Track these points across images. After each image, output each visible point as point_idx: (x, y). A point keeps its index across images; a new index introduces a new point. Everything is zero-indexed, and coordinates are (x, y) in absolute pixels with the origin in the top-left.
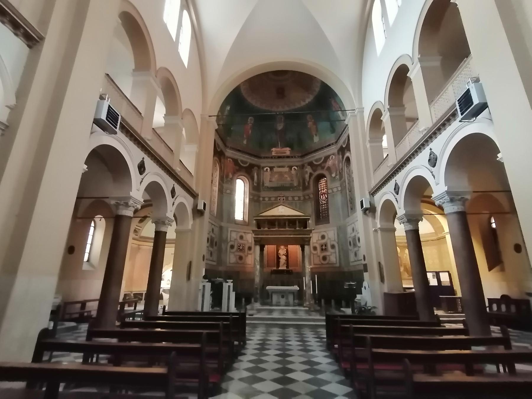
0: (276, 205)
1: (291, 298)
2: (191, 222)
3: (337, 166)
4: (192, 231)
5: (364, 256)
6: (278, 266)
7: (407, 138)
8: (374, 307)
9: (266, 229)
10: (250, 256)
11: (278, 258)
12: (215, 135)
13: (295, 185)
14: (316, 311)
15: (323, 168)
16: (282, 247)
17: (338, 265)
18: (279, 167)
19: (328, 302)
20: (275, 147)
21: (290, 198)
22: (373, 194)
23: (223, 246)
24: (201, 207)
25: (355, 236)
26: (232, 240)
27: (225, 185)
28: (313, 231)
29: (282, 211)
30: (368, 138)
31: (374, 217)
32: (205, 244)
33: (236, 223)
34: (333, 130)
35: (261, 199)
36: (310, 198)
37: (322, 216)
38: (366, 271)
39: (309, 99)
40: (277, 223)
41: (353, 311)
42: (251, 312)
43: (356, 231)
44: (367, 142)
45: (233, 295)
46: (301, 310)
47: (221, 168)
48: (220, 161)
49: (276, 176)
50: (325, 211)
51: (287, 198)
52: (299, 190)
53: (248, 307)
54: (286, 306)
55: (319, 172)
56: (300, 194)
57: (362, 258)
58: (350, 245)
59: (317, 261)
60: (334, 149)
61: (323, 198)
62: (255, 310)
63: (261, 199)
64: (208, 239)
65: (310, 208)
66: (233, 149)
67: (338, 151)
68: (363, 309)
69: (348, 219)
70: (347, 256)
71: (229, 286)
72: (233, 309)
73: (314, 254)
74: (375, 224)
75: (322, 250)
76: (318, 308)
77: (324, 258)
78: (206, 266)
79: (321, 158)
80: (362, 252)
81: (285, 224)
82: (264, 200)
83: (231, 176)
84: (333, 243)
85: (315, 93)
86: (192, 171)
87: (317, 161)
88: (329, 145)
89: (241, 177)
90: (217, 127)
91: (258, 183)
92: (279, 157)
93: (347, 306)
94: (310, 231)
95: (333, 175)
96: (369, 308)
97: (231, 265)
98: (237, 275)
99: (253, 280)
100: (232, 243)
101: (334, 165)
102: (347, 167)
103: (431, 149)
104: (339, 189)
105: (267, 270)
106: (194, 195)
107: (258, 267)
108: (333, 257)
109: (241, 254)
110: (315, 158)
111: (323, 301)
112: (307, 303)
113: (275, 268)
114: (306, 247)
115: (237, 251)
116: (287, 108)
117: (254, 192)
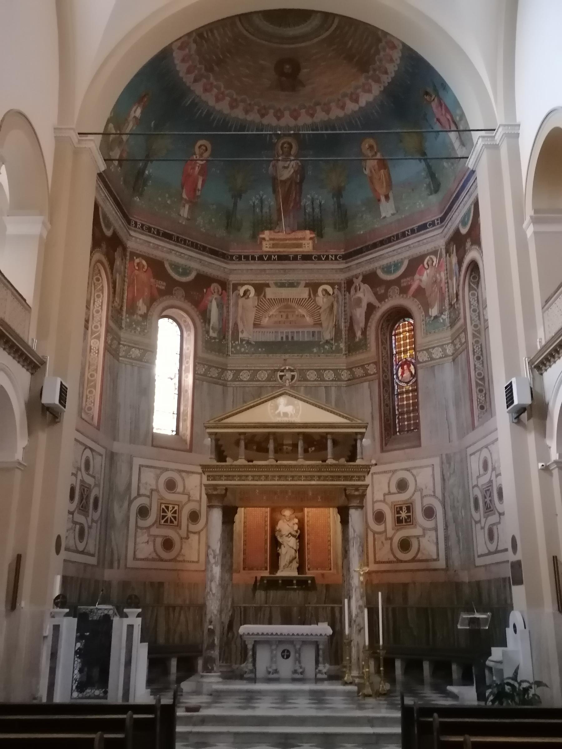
0: (270, 395)
1: (309, 655)
2: (22, 442)
4: (26, 468)
5: (514, 540)
6: (275, 566)
8: (539, 684)
9: (242, 461)
10: (194, 538)
11: (276, 544)
12: (98, 189)
13: (327, 336)
14: (378, 694)
15: (404, 291)
16: (287, 513)
17: (442, 564)
18: (282, 285)
19: (413, 667)
20: (271, 229)
21: (311, 375)
22: (540, 365)
23: (118, 515)
24: (51, 397)
25: (491, 481)
26: (142, 491)
27: (124, 335)
28: (373, 469)
29: (287, 410)
30: (529, 211)
31: (542, 431)
32: (63, 504)
33: (157, 442)
34: (435, 187)
36: (367, 375)
37: (398, 425)
38: (518, 581)
40: (271, 446)
41: (481, 696)
42: (194, 701)
43: (494, 469)
45: (141, 653)
46: (334, 693)
48: (112, 263)
49: (273, 311)
50: (408, 412)
51: (302, 372)
52: (339, 351)
53: (186, 686)
54: (294, 680)
55: (395, 300)
57: (509, 546)
59: (384, 554)
60: (436, 239)
61: (403, 375)
62: (205, 695)
63: (230, 375)
64: (72, 490)
65: (365, 406)
67: (448, 244)
68: (507, 688)
69: (472, 436)
70: (468, 542)
71: (130, 627)
72: (141, 694)
73: (374, 533)
74: (543, 452)
75: (399, 521)
76: (387, 687)
77: (405, 545)
78: (65, 568)
79: (402, 262)
80: (509, 527)
81: (295, 446)
82: (236, 378)
84: (428, 501)
85: (386, 79)
86: (27, 290)
87: (387, 269)
88: (423, 227)
90: (102, 167)
91: (223, 332)
92: (282, 258)
93: (466, 680)
94: (367, 469)
95: (434, 312)
96: (525, 685)
97: (139, 564)
98: (153, 595)
99: (201, 609)
102: (471, 288)
104: (449, 350)
105: (245, 578)
106: (33, 364)
107: (217, 570)
108: (430, 541)
109: (170, 533)
110: (385, 262)
111: (398, 664)
112: (355, 673)
113: (266, 574)
114: (354, 515)
115: (157, 523)
116: (304, 119)
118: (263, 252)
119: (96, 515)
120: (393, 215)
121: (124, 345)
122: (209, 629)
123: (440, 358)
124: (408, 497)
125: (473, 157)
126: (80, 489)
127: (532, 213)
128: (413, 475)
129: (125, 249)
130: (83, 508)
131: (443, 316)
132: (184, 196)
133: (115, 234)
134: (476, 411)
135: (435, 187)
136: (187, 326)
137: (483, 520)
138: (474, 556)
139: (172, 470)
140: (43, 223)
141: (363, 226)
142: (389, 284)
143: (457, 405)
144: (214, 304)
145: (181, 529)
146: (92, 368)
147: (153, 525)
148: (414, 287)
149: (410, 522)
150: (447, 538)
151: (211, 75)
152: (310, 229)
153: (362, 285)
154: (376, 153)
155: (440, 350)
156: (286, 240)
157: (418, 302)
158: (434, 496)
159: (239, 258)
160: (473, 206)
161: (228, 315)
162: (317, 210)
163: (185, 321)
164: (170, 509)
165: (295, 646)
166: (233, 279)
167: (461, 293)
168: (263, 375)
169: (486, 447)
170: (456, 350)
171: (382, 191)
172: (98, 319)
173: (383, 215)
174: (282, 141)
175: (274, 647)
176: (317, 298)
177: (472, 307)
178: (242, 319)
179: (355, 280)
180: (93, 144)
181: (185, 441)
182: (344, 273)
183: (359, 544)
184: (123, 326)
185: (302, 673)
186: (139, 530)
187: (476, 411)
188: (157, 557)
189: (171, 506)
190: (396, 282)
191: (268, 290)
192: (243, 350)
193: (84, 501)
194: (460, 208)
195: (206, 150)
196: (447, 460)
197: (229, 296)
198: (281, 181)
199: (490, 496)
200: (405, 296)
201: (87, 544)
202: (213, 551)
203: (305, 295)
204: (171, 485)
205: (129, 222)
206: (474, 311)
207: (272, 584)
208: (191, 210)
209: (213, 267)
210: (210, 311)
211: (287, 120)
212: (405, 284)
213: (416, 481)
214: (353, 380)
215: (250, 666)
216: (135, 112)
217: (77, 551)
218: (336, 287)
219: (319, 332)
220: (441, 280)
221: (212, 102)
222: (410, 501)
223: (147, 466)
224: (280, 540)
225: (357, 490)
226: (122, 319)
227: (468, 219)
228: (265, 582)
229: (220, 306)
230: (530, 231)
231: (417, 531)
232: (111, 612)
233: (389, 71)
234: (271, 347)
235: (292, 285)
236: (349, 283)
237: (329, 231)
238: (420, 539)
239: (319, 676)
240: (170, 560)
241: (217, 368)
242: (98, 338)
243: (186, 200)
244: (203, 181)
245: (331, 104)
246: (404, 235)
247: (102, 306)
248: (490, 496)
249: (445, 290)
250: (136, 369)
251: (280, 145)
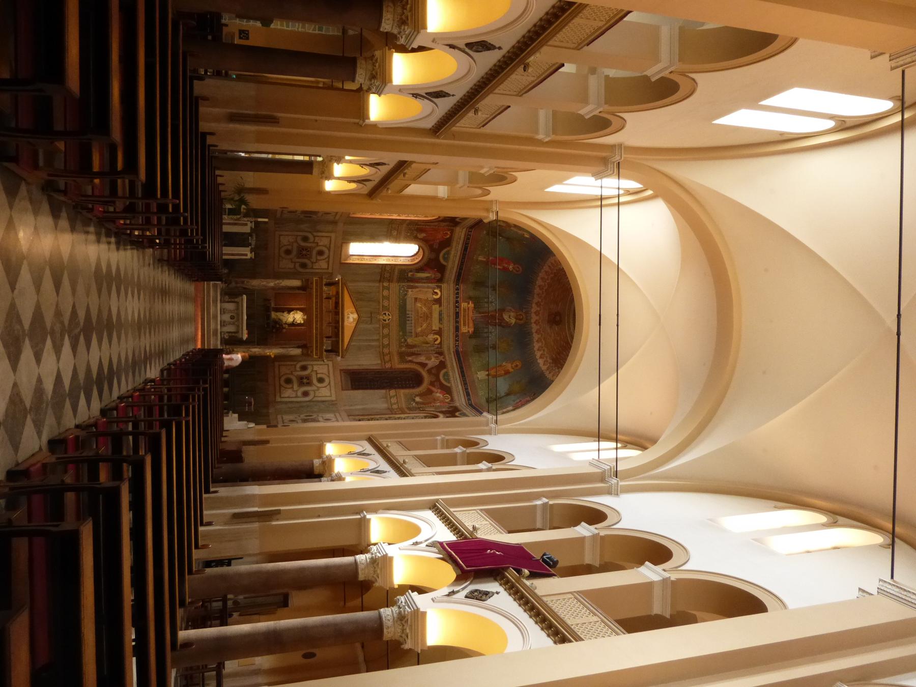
1: (231, 329)
7: (595, 619)
15: (432, 384)
18: (440, 314)
21: (386, 331)
23: (303, 226)
26: (317, 238)
29: (351, 318)
35: (386, 284)
44: (545, 500)
52: (401, 347)
56: (394, 349)
66: (467, 238)
83: (423, 235)
84: (312, 393)
85: (547, 373)
87: (446, 374)
89: (421, 253)
92: (457, 315)
95: (418, 399)
100: (312, 239)
101: (435, 400)
103: (497, 593)
104: (395, 406)
110: (451, 374)
113: (273, 305)
117: (396, 273)
127: (673, 579)
141: (475, 361)
143: (363, 409)
148: (433, 389)
150: (292, 402)
159: (457, 289)
168: (386, 304)
180: (492, 217)
190: (438, 379)
203: (434, 328)
204: (321, 253)
207: (268, 310)
208: (481, 261)
211: (534, 318)
214: (382, 355)
229: (427, 278)
230: (539, 502)
231: (296, 387)
234: (403, 309)
235: (440, 320)
236: (441, 353)
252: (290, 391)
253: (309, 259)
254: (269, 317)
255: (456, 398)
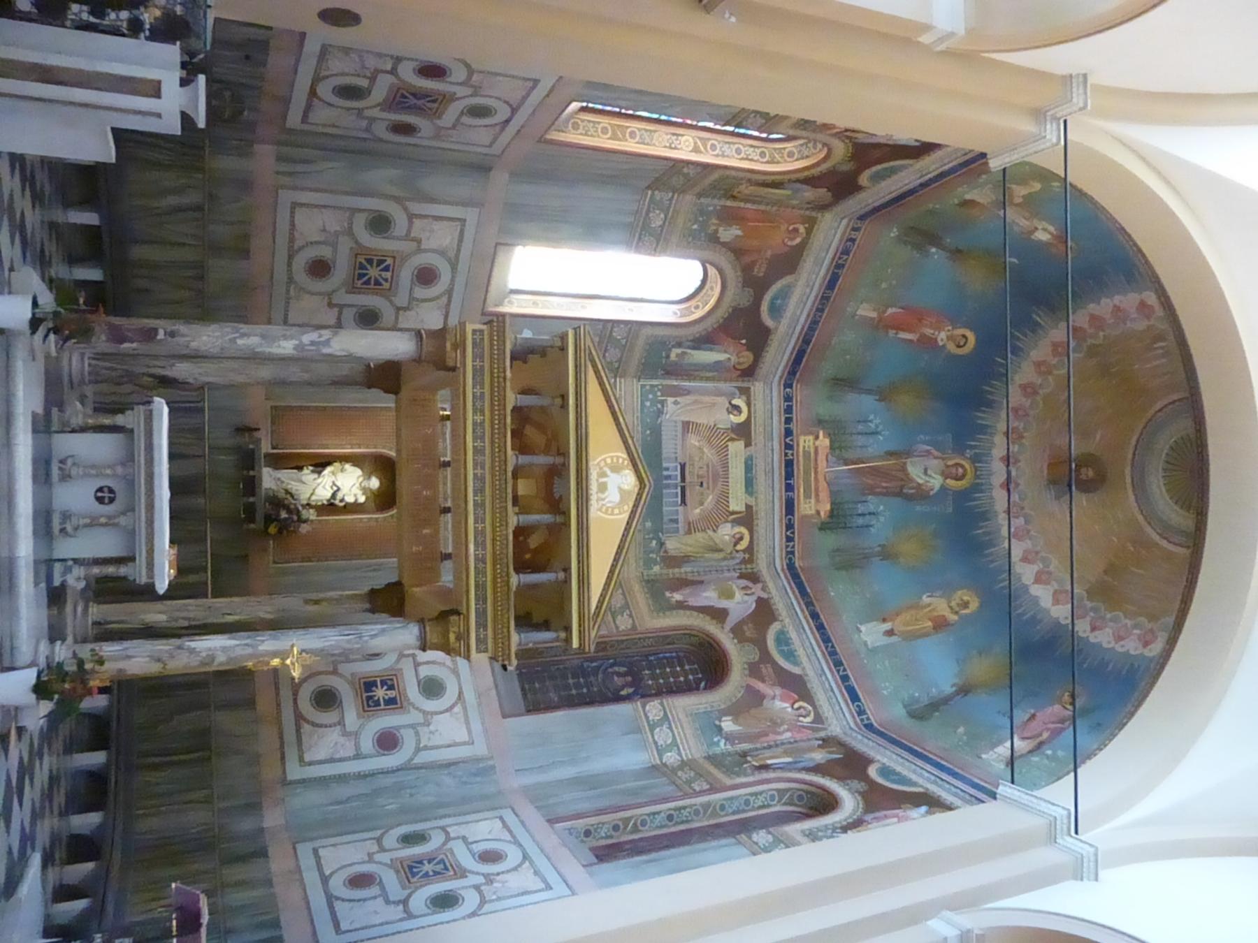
1: (102, 544)
3: (772, 738)
15: (754, 670)
18: (749, 467)
20: (832, 448)
23: (382, 176)
25: (461, 873)
39: (1047, 600)
47: (775, 182)
48: (811, 181)
49: (709, 454)
52: (648, 563)
58: (408, 840)
71: (154, 89)
75: (369, 685)
79: (796, 663)
83: (729, 233)
87: (782, 639)
88: (854, 697)
92: (789, 464)
95: (728, 725)
101: (775, 724)
104: (671, 758)
110: (793, 635)
113: (266, 447)
117: (641, 342)
118: (798, 436)
119: (381, 130)
120: (865, 644)
121: (671, 200)
122: (155, 331)
123: (656, 743)
124: (412, 700)
125: (1016, 793)
126: (439, 93)
128: (452, 707)
129: (824, 207)
130: (401, 99)
131: (723, 741)
132: (890, 311)
133: (859, 188)
134: (581, 824)
135: (922, 712)
136: (688, 312)
137: (385, 858)
138: (316, 838)
139: (453, 280)
140: (952, 34)
141: (841, 595)
142: (761, 643)
144: (721, 357)
145: (347, 292)
146: (646, 135)
147: (357, 242)
148: (760, 686)
149: (369, 706)
150: (342, 779)
151: (1081, 355)
152: (832, 510)
153: (754, 598)
154: (956, 613)
155: (669, 742)
156: (816, 473)
157: (739, 695)
158: (418, 750)
159: (788, 398)
160: (921, 790)
161: (701, 379)
162: (860, 521)
163: (697, 307)
164: (383, 274)
165: (124, 513)
166: (757, 388)
167: (772, 775)
169: (526, 857)
170: (674, 770)
171: (898, 625)
172: (728, 152)
173: (863, 628)
174: (967, 466)
175: (119, 470)
176: (729, 525)
177: (752, 799)
178: (696, 402)
179: (760, 585)
181: (500, 304)
182: (768, 567)
183: (348, 646)
184: (702, 200)
185: (63, 530)
186: (347, 214)
187: (581, 824)
188: (296, 247)
189: (388, 275)
190: (766, 656)
191: (741, 444)
192: (648, 404)
193: (413, 101)
194: (907, 764)
195: (959, 346)
196: (481, 769)
197: (731, 380)
198: (905, 464)
199: (436, 873)
200: (747, 672)
201: (329, 104)
202: (328, 341)
204: (426, 276)
205: (862, 218)
206: (747, 803)
207: (248, 460)
208: (865, 319)
209: (778, 356)
210: (711, 350)
212: (764, 670)
213: (441, 713)
215: (77, 421)
216: (1045, 230)
217: (316, 80)
218: (747, 556)
219: (677, 530)
220: (779, 733)
221: (1035, 355)
222: (405, 704)
223: (462, 232)
224: (329, 469)
225: (458, 638)
226: (714, 197)
227: (894, 782)
228: (251, 446)
231: (351, 717)
232: (195, 44)
233: (1097, 633)
235: (749, 484)
236: (754, 578)
237: (830, 540)
238: (338, 727)
239: (58, 568)
240: (290, 270)
241: (620, 361)
242: (696, 150)
243: (884, 312)
244: (911, 341)
245: (1029, 542)
246: (838, 664)
247: (747, 159)
248: (436, 873)
249: (764, 741)
250: (630, 219)
251: (963, 462)
252: (334, 735)
253: (388, 294)
254: (251, 485)
255: (826, 710)
